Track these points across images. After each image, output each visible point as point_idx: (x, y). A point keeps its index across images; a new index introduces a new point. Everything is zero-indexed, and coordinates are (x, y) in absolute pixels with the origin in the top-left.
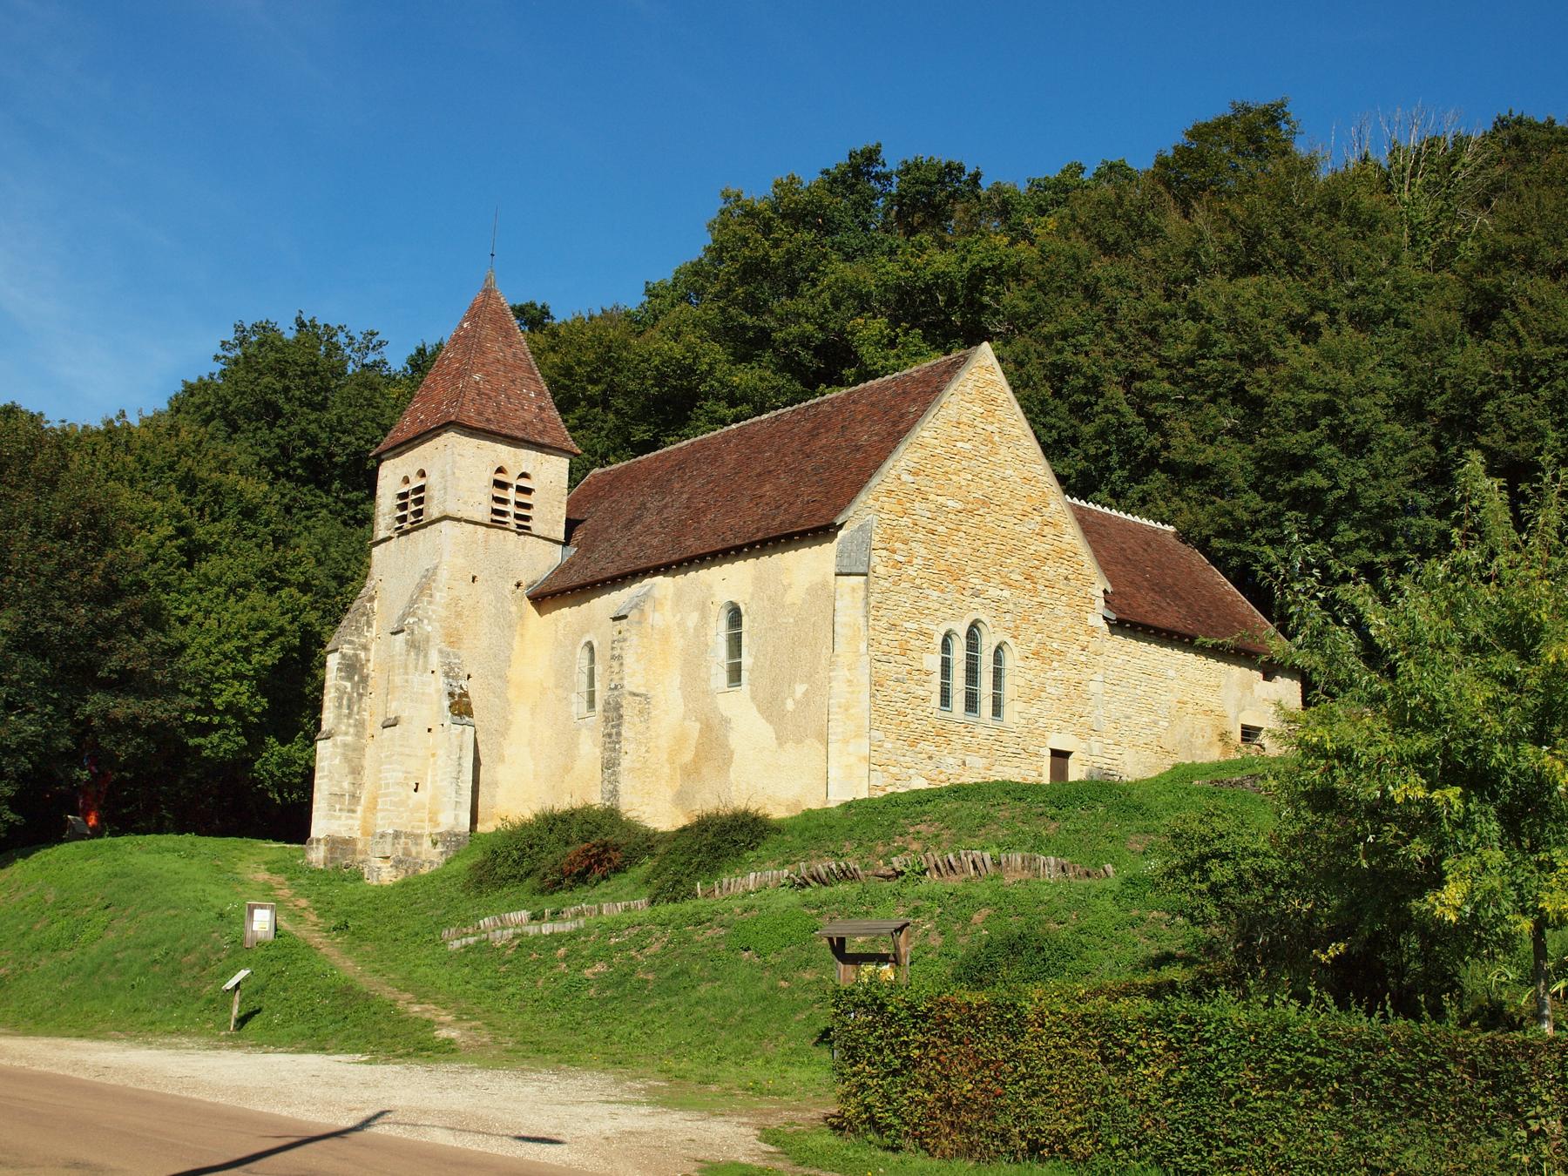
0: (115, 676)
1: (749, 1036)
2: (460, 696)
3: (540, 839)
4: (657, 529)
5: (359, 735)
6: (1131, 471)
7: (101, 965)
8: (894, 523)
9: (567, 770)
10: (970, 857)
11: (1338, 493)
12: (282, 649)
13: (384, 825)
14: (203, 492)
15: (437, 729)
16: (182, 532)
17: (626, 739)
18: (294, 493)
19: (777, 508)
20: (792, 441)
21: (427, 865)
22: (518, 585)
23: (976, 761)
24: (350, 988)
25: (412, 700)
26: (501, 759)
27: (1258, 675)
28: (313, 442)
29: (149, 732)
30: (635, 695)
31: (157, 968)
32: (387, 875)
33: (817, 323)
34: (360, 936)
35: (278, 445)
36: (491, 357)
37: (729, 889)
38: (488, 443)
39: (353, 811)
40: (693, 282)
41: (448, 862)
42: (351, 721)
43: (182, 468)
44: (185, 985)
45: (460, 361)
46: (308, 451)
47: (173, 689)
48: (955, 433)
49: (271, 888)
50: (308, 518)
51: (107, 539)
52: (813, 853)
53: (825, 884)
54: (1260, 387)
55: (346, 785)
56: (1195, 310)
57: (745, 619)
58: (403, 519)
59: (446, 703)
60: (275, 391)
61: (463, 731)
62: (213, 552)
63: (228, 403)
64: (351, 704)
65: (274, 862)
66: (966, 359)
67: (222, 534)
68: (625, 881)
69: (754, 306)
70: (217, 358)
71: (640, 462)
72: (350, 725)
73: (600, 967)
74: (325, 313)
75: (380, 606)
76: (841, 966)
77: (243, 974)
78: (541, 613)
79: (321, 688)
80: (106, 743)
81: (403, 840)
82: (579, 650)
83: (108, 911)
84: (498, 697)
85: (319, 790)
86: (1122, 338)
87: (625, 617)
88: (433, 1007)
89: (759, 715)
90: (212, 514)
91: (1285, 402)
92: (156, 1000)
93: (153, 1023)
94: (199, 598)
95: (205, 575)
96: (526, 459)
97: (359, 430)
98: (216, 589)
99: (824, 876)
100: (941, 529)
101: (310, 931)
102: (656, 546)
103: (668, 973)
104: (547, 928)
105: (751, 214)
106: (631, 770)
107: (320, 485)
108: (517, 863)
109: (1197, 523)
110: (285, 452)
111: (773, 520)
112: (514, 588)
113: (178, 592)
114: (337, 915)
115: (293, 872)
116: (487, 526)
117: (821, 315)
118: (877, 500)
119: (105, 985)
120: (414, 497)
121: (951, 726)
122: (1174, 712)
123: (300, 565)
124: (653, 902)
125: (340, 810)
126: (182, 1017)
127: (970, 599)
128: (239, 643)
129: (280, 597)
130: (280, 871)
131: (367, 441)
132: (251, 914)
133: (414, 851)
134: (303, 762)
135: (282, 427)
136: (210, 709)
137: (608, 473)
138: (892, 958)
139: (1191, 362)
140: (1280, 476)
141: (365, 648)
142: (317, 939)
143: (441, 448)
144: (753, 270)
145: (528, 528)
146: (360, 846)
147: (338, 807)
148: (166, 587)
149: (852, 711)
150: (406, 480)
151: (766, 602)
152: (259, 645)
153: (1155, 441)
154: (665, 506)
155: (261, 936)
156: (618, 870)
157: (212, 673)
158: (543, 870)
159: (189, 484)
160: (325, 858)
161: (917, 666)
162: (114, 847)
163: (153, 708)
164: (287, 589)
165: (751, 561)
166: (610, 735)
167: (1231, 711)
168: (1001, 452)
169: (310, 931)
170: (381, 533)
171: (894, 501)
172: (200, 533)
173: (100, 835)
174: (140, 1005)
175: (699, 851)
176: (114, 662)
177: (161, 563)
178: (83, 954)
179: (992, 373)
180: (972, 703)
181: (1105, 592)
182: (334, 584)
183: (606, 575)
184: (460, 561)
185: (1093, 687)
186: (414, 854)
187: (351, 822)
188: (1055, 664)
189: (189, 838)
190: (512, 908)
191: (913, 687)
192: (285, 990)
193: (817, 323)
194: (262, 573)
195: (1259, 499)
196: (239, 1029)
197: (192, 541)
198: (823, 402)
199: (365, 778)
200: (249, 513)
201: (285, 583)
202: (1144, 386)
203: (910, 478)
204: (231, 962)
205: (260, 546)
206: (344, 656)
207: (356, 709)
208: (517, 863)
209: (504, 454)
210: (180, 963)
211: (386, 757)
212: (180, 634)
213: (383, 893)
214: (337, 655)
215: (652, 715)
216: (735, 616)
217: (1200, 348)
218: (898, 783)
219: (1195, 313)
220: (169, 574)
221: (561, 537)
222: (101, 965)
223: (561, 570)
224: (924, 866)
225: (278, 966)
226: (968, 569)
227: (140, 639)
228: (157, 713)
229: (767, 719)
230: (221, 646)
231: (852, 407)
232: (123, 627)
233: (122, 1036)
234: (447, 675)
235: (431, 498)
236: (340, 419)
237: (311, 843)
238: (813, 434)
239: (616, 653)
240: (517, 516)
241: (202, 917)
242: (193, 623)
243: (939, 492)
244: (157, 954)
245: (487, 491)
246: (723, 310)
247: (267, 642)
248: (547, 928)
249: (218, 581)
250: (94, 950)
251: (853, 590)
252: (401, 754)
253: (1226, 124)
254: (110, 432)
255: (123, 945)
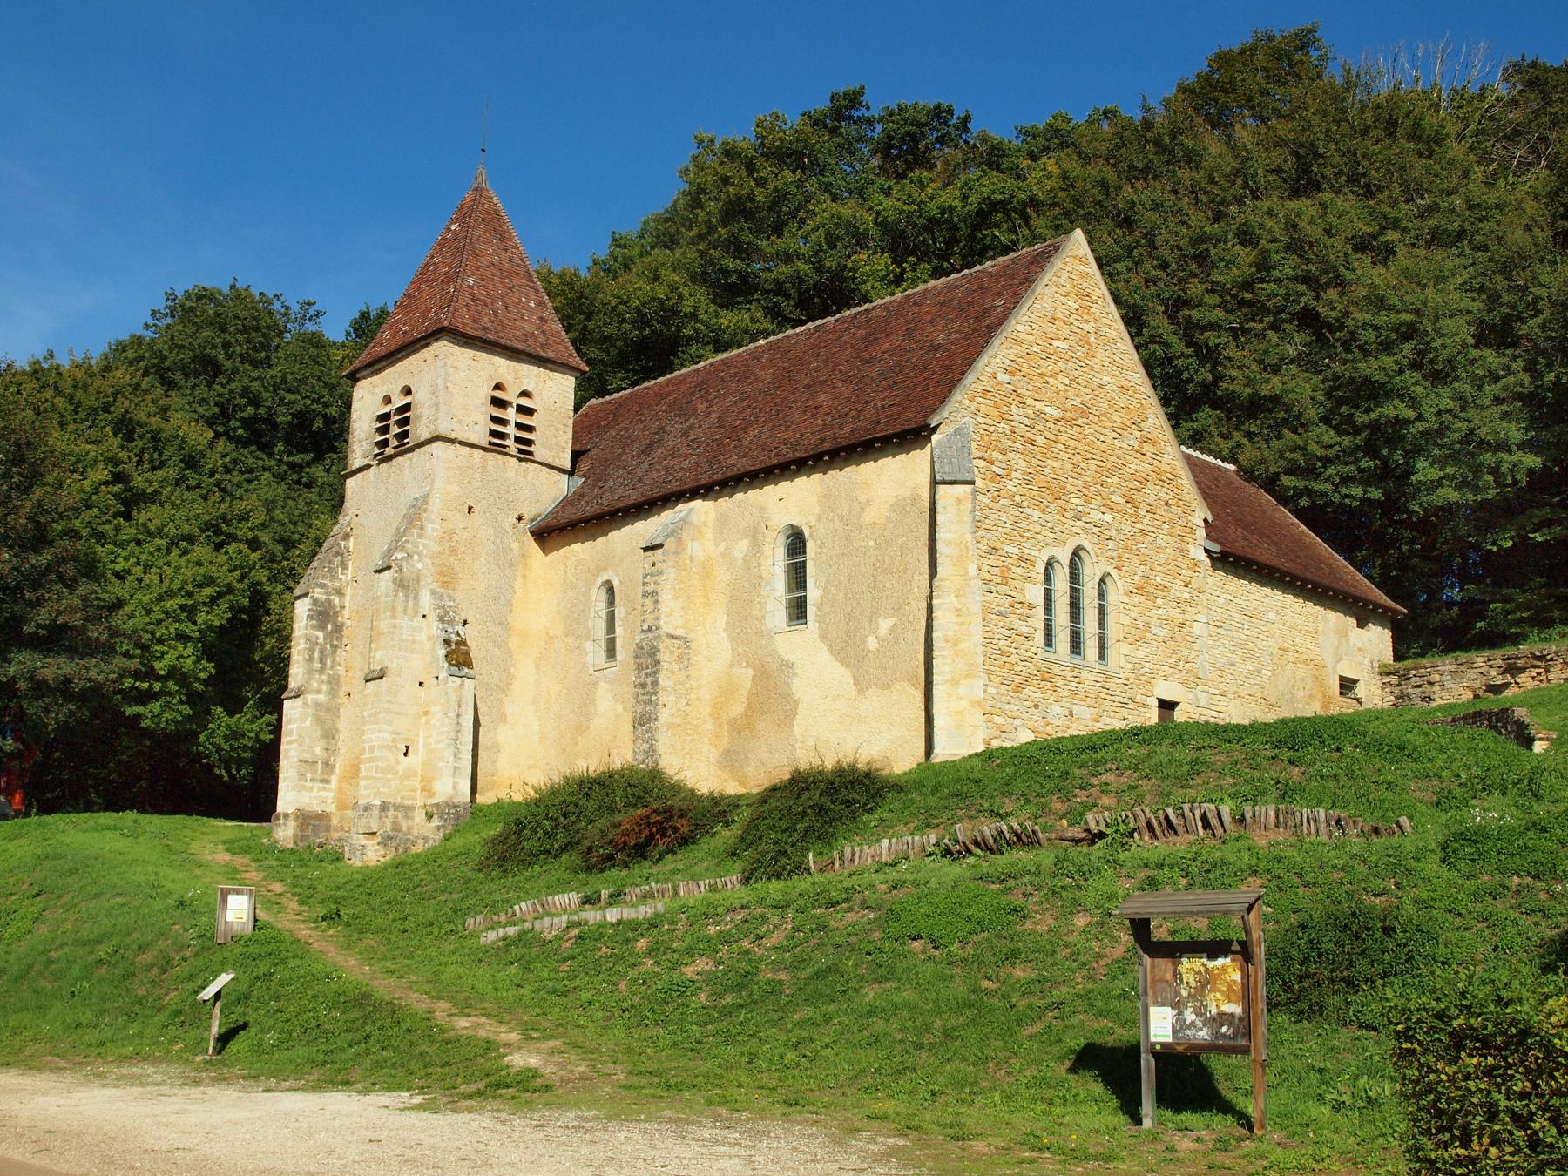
0: (44, 632)
1: (964, 1059)
2: (457, 643)
3: (576, 805)
4: (684, 450)
5: (333, 693)
6: (1177, 407)
7: (31, 966)
8: (991, 429)
9: (581, 730)
10: (1198, 813)
11: (1421, 426)
12: (231, 608)
13: (368, 794)
14: (141, 437)
15: (430, 683)
16: (119, 478)
17: (665, 689)
18: (233, 455)
19: (842, 416)
20: (843, 348)
21: (421, 842)
22: (520, 519)
23: (1083, 712)
24: (367, 995)
25: (400, 649)
26: (503, 718)
27: (1352, 621)
28: (256, 401)
29: (83, 697)
30: (673, 637)
31: (103, 970)
32: (373, 854)
33: (811, 262)
34: (357, 928)
35: (216, 404)
36: (485, 260)
37: (852, 860)
38: (485, 355)
39: (327, 781)
40: (665, 234)
41: (447, 838)
42: (324, 677)
43: (117, 411)
44: (141, 992)
45: (449, 265)
46: (250, 410)
47: (108, 650)
48: (1051, 329)
49: (235, 871)
50: (249, 481)
51: (34, 477)
52: (960, 813)
53: (992, 852)
54: (1333, 309)
55: (318, 751)
56: (1244, 233)
57: (810, 546)
58: (384, 443)
59: (442, 651)
60: (214, 347)
61: (462, 684)
62: (153, 502)
63: (164, 358)
64: (323, 657)
65: (234, 841)
66: (1057, 249)
67: (163, 482)
68: (700, 855)
69: (738, 248)
70: (147, 326)
71: (646, 388)
72: (322, 682)
73: (703, 964)
74: (258, 283)
75: (357, 544)
76: (1147, 960)
77: (224, 979)
78: (546, 551)
79: (286, 640)
80: (33, 709)
81: (391, 813)
82: (594, 591)
83: (39, 898)
84: (499, 647)
85: (287, 757)
86: (1164, 266)
87: (660, 546)
88: (484, 1020)
89: (830, 658)
90: (151, 461)
91: (1364, 324)
92: (103, 1012)
93: (102, 1044)
94: (137, 550)
95: (144, 525)
96: (520, 376)
97: (304, 389)
98: (158, 541)
99: (991, 841)
100: (1040, 439)
101: (293, 921)
102: (686, 469)
103: (810, 971)
104: (613, 914)
105: (730, 153)
106: (670, 726)
107: (262, 448)
108: (549, 835)
109: (1263, 461)
110: (225, 413)
111: (841, 428)
112: (515, 521)
113: (115, 544)
114: (322, 902)
115: (262, 853)
116: (484, 449)
117: (816, 253)
118: (972, 400)
119: (37, 992)
120: (397, 418)
121: (1056, 670)
122: (1276, 661)
123: (247, 520)
124: (747, 880)
125: (312, 780)
126: (140, 1035)
127: (1071, 523)
128: (183, 601)
129: (227, 552)
130: (243, 851)
131: (314, 401)
132: (224, 900)
133: (404, 825)
134: (252, 735)
135: (223, 386)
136: (149, 674)
137: (610, 402)
138: (1236, 947)
139: (1248, 286)
140: (1357, 407)
141: (339, 593)
142: (304, 932)
143: (430, 359)
144: (737, 210)
145: (530, 453)
146: (335, 822)
147: (309, 776)
148: (101, 538)
149: (962, 646)
150: (388, 400)
151: (837, 523)
152: (205, 604)
153: (1205, 374)
154: (691, 428)
155: (237, 929)
156: (685, 841)
157: (153, 633)
158: (586, 843)
159: (126, 428)
160: (295, 835)
161: (1020, 598)
162: (44, 826)
163: (88, 669)
164: (235, 545)
165: (816, 477)
166: (643, 685)
167: (1329, 661)
168: (1098, 355)
169: (293, 921)
170: (356, 461)
171: (991, 403)
172: (138, 481)
173: (27, 815)
174: (84, 1020)
175: (804, 814)
176: (43, 616)
177: (95, 511)
178: (8, 953)
179: (1086, 265)
180: (1076, 645)
181: (1205, 520)
182: (280, 548)
183: (632, 500)
184: (454, 489)
185: (1198, 629)
186: (404, 829)
187: (323, 794)
188: (1159, 601)
189: (130, 816)
190: (552, 889)
191: (1017, 623)
192: (277, 999)
193: (811, 262)
194: (209, 526)
195: (1332, 432)
196: (219, 1052)
197: (130, 489)
198: (875, 308)
199: (340, 743)
200: (191, 462)
201: (232, 538)
202: (1195, 314)
203: (1006, 378)
204: (199, 962)
205: (205, 498)
206: (315, 601)
207: (329, 663)
208: (549, 835)
209: (502, 367)
210: (133, 963)
211: (370, 715)
212: (116, 589)
213: (369, 880)
214: (307, 600)
215: (692, 661)
216: (797, 542)
217: (1258, 271)
218: (1003, 735)
219: (1246, 237)
220: (104, 524)
221: (567, 465)
222: (31, 966)
223: (567, 502)
224: (1132, 825)
225: (262, 968)
226: (1069, 488)
227: (71, 588)
228: (93, 674)
229: (842, 661)
230: (162, 604)
231: (915, 309)
232: (53, 576)
233: (62, 1064)
234: (441, 619)
235: (419, 417)
236: (284, 380)
237: (278, 818)
238: (870, 340)
239: (649, 589)
240: (518, 440)
241: (158, 905)
242: (130, 578)
243: (1037, 396)
244: (102, 952)
245: (484, 409)
246: (702, 254)
247: (213, 600)
248: (613, 914)
249: (160, 533)
250: (22, 948)
251: (959, 501)
252: (389, 711)
253: (1249, 51)
254: (36, 372)
255: (59, 942)
